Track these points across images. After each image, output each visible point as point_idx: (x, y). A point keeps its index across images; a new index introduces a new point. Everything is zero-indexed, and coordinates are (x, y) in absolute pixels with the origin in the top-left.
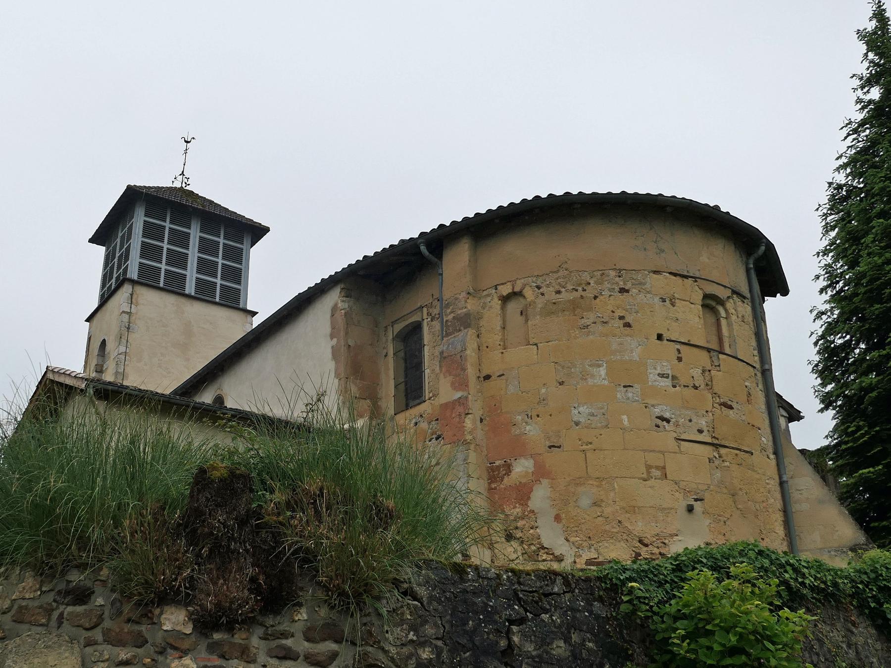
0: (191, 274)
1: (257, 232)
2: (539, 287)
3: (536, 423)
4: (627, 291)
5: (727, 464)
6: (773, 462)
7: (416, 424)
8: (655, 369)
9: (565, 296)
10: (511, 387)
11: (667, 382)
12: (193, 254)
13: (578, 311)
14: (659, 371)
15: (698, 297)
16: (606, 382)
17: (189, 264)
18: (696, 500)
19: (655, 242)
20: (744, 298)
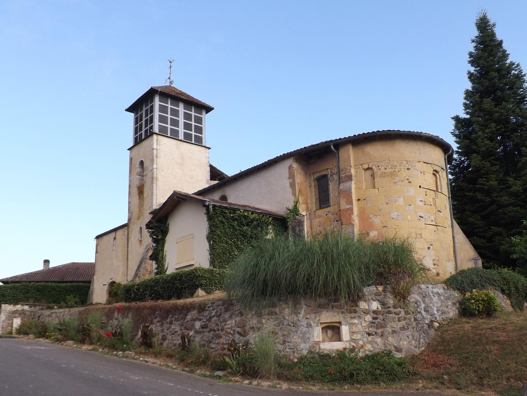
0: (181, 130)
2: (378, 166)
3: (378, 218)
4: (410, 169)
5: (440, 232)
6: (451, 230)
7: (326, 215)
8: (419, 198)
9: (388, 170)
10: (368, 204)
11: (422, 203)
12: (181, 120)
13: (393, 176)
14: (420, 200)
15: (432, 172)
16: (403, 204)
17: (158, 117)
18: (431, 245)
19: (419, 150)
20: (444, 170)
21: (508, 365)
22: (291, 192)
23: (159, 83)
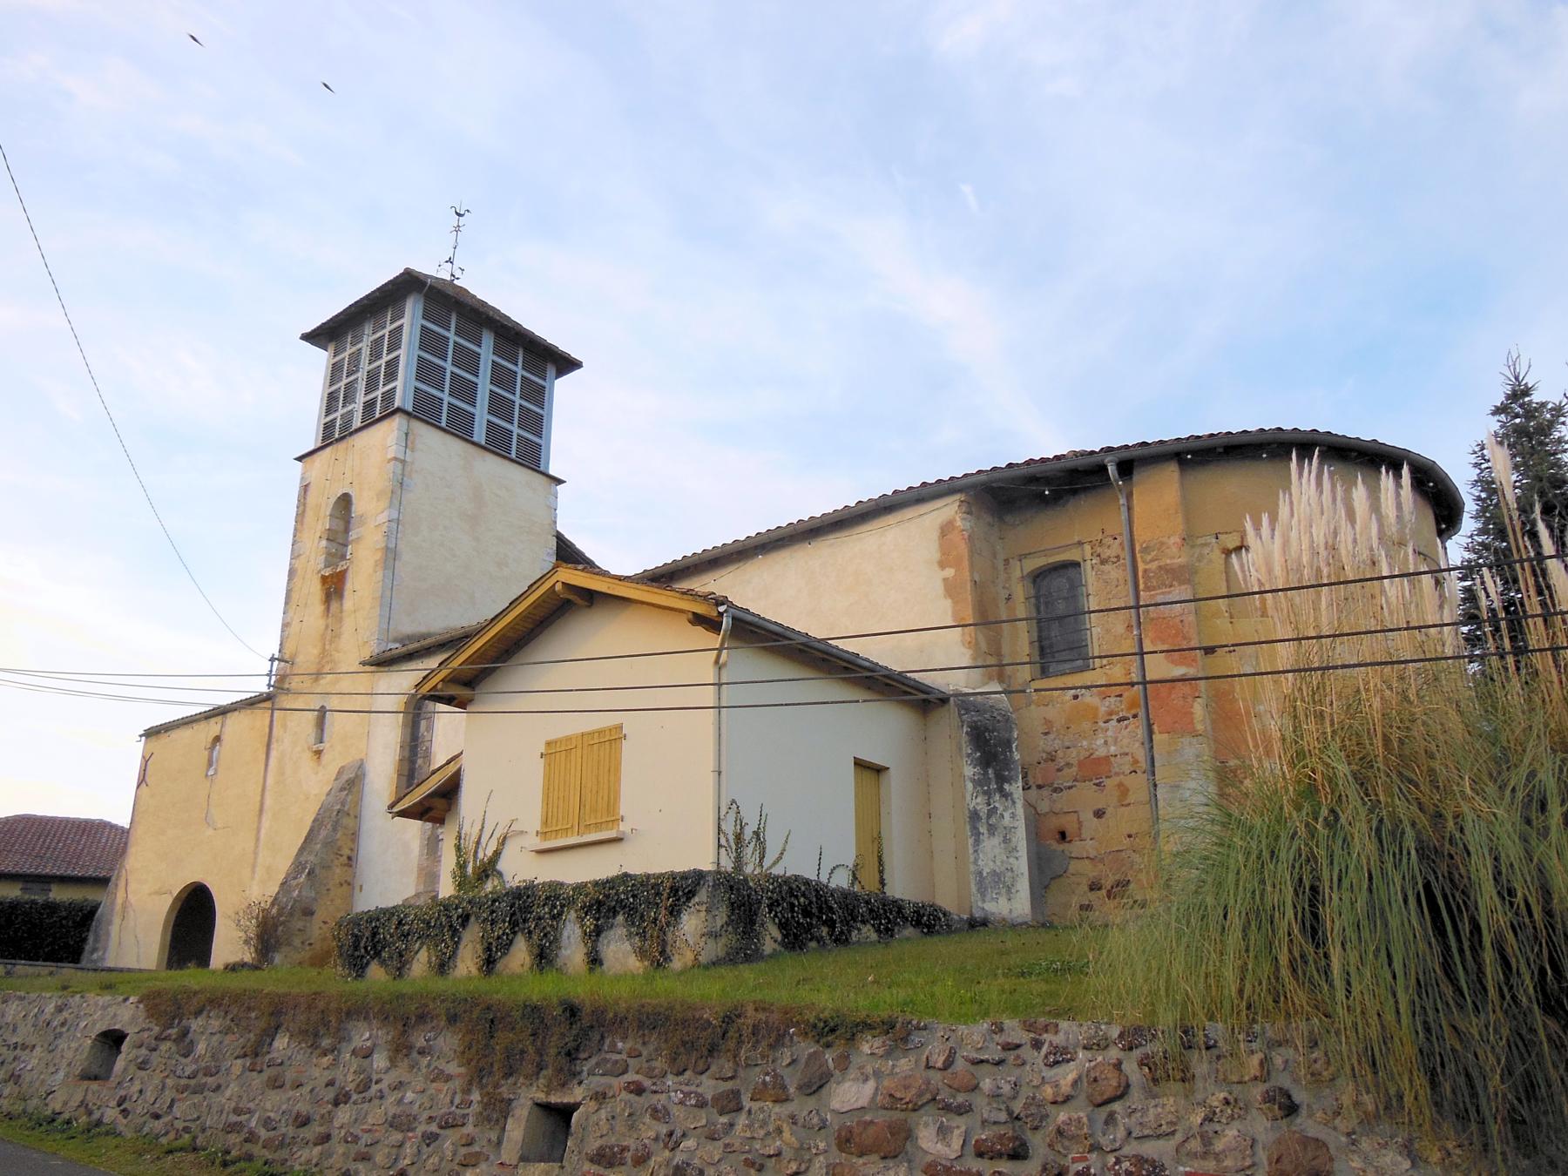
1: (566, 364)
12: (484, 385)
21: (654, 1084)
22: (950, 613)
23: (430, 266)
